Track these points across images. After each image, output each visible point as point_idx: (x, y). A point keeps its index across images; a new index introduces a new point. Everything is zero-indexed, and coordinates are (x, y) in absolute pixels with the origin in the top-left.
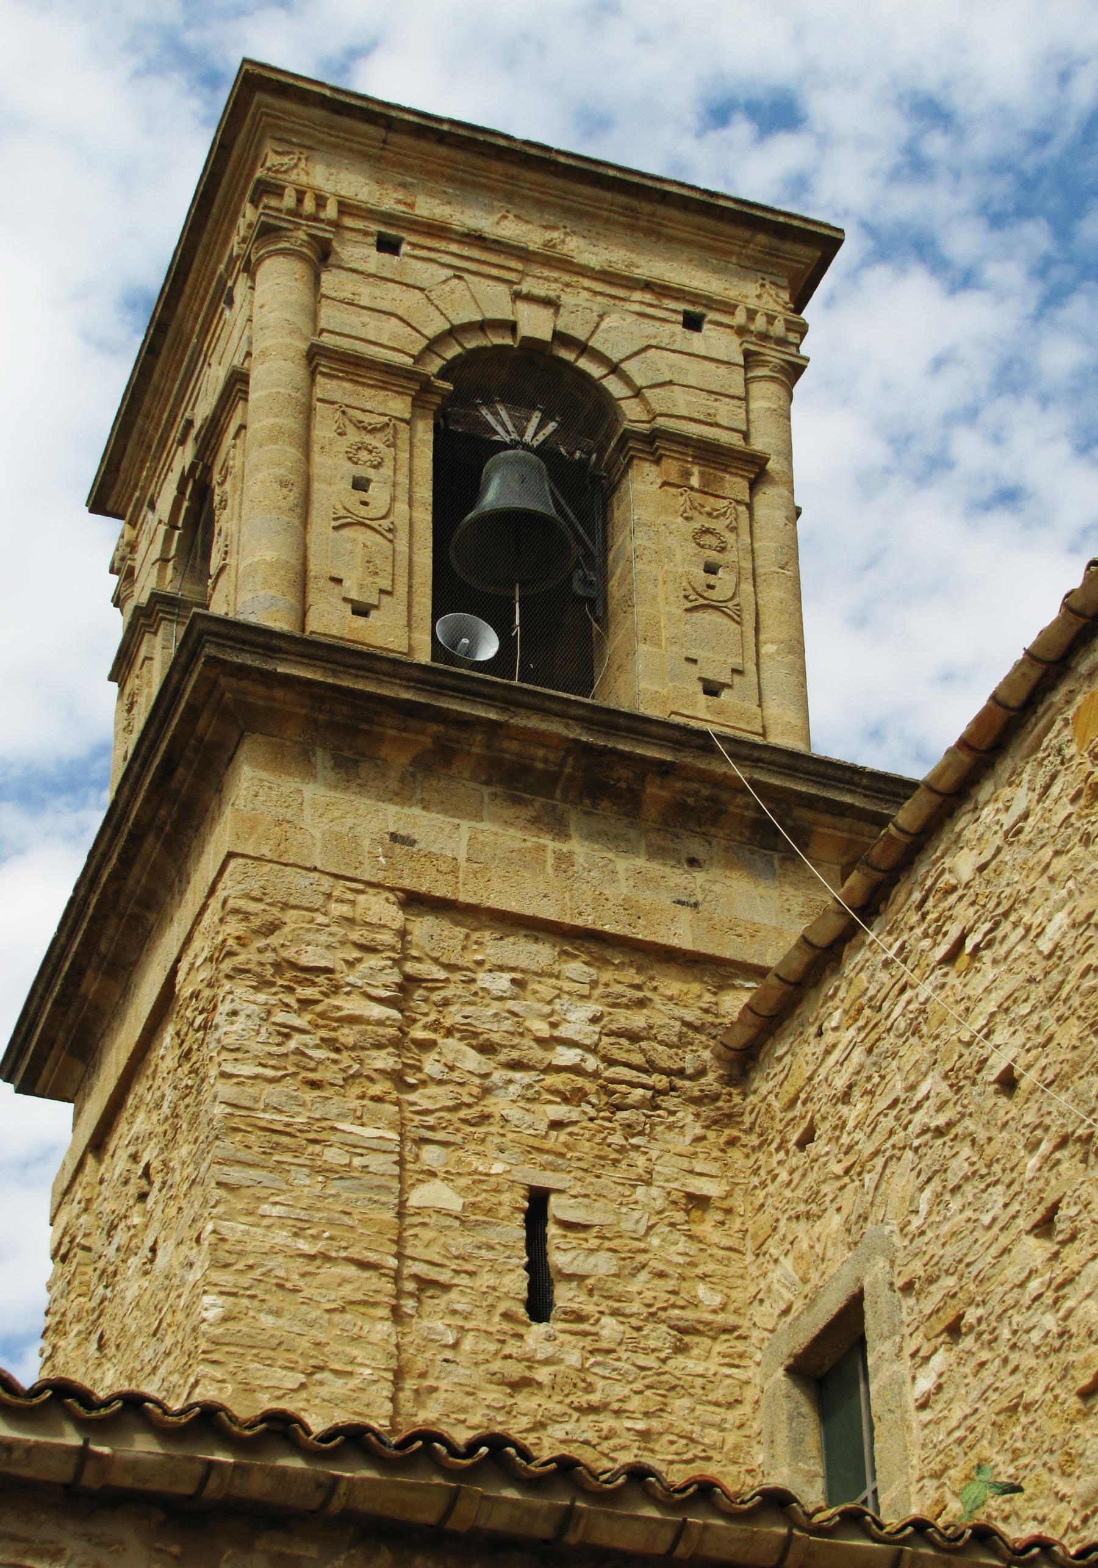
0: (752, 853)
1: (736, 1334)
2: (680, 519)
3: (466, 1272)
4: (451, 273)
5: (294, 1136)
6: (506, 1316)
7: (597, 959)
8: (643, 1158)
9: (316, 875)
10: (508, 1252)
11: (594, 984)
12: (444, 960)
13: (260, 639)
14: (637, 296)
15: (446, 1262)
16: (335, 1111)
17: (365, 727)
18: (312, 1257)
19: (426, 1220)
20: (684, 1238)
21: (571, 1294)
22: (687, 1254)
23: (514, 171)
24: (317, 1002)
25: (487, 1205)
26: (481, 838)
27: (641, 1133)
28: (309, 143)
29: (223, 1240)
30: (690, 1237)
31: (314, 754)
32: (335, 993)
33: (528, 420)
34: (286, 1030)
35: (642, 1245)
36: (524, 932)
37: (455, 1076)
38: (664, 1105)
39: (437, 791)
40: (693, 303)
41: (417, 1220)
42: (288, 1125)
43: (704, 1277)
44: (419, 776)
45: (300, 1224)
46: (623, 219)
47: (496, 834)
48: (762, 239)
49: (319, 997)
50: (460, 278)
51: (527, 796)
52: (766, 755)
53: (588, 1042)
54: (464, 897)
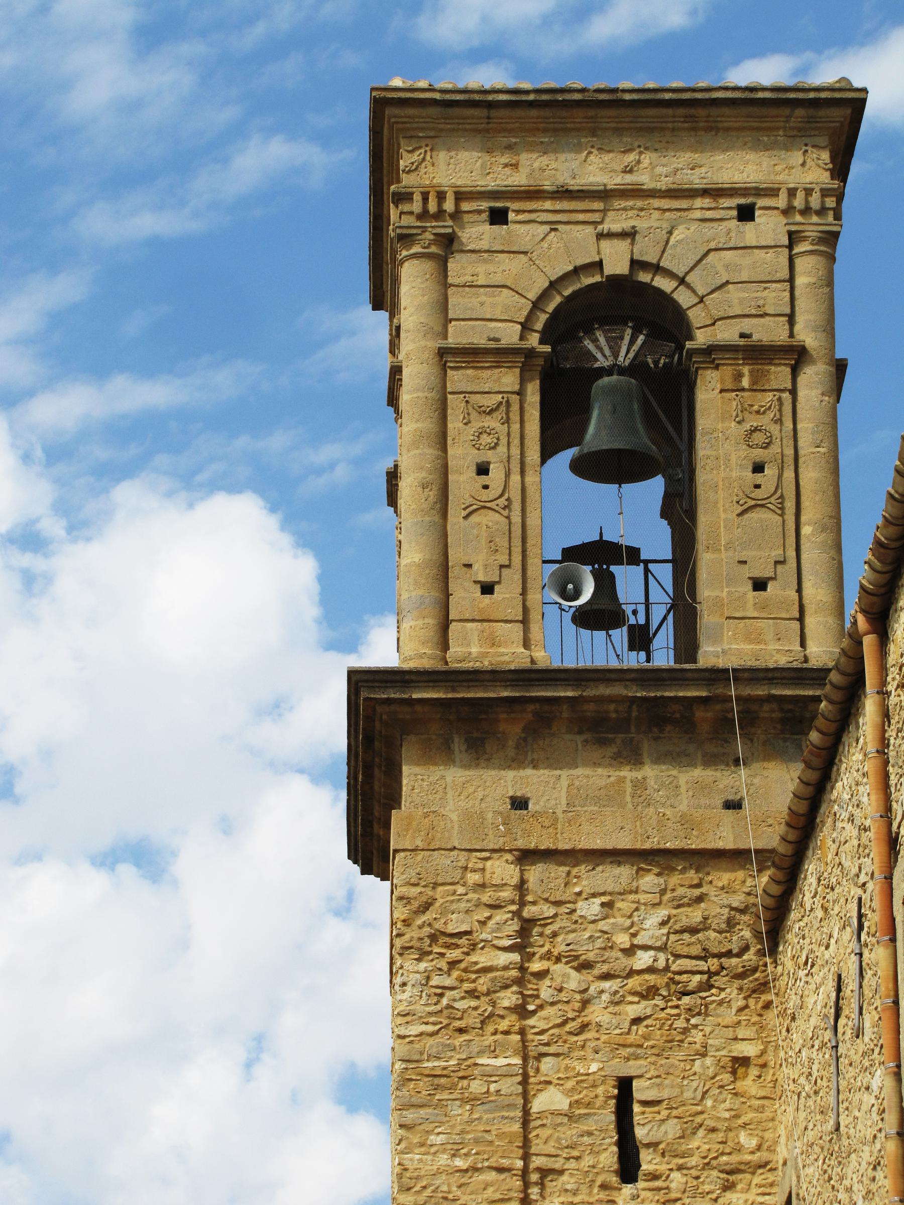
0: (785, 740)
1: (768, 1167)
2: (733, 424)
3: (573, 1158)
4: (546, 228)
5: (449, 1077)
6: (604, 1187)
7: (666, 868)
8: (701, 1034)
9: (455, 853)
10: (603, 1135)
11: (663, 892)
12: (552, 899)
13: (397, 677)
14: (699, 202)
15: (559, 1152)
16: (476, 1050)
17: (484, 716)
18: (466, 1171)
19: (545, 1122)
20: (730, 1096)
21: (649, 1158)
22: (732, 1109)
23: (591, 113)
24: (460, 961)
25: (587, 1100)
26: (577, 783)
27: (699, 1014)
28: (432, 134)
29: (406, 1170)
30: (736, 1094)
31: (453, 742)
32: (473, 950)
33: (622, 338)
34: (439, 991)
35: (699, 1108)
36: (609, 860)
37: (563, 996)
38: (717, 984)
39: (543, 749)
40: (744, 196)
41: (539, 1122)
42: (445, 1068)
43: (745, 1126)
44: (530, 739)
45: (456, 1147)
46: (686, 125)
47: (588, 777)
48: (800, 112)
49: (461, 957)
50: (556, 230)
51: (610, 736)
52: (777, 675)
53: (658, 944)
54: (563, 846)
